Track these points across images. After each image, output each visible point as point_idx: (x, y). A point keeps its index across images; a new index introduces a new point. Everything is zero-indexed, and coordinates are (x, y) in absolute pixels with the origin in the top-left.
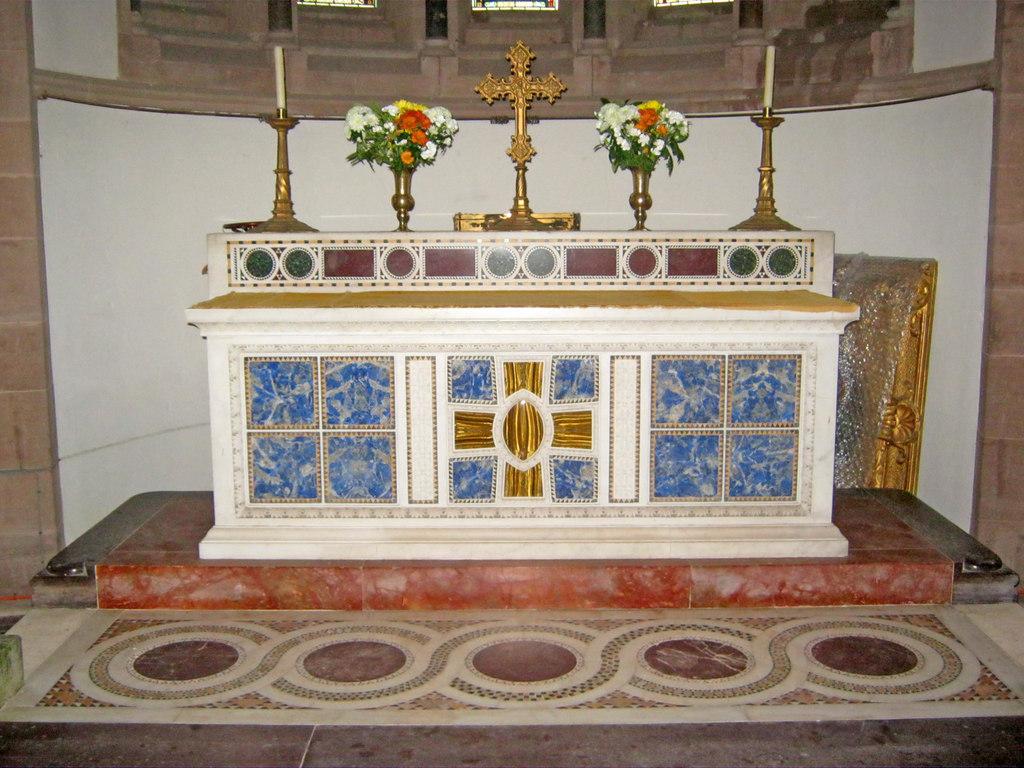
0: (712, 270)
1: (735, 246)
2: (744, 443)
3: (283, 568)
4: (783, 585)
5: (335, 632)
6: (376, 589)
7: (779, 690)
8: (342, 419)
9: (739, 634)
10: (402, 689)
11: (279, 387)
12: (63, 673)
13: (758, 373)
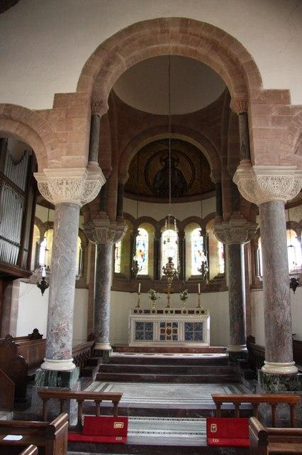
3: (139, 348)
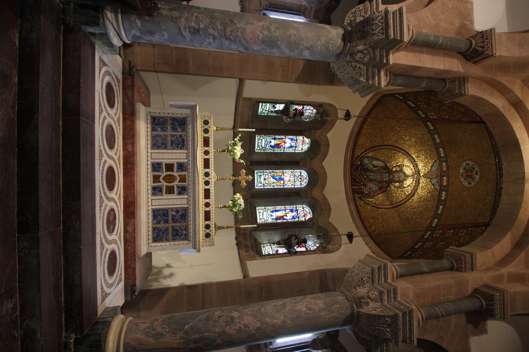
0: (206, 220)
1: (211, 225)
2: (167, 229)
4: (130, 242)
5: (118, 133)
6: (129, 144)
7: (104, 241)
8: (172, 138)
9: (118, 232)
10: (104, 148)
11: (180, 124)
12: (107, 64)
13: (184, 231)
